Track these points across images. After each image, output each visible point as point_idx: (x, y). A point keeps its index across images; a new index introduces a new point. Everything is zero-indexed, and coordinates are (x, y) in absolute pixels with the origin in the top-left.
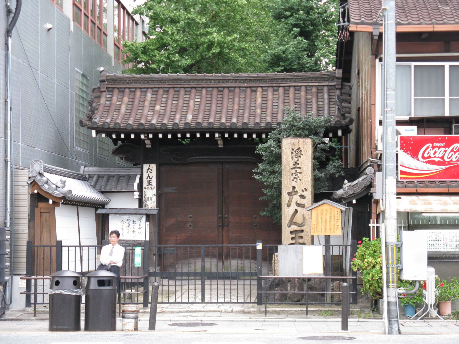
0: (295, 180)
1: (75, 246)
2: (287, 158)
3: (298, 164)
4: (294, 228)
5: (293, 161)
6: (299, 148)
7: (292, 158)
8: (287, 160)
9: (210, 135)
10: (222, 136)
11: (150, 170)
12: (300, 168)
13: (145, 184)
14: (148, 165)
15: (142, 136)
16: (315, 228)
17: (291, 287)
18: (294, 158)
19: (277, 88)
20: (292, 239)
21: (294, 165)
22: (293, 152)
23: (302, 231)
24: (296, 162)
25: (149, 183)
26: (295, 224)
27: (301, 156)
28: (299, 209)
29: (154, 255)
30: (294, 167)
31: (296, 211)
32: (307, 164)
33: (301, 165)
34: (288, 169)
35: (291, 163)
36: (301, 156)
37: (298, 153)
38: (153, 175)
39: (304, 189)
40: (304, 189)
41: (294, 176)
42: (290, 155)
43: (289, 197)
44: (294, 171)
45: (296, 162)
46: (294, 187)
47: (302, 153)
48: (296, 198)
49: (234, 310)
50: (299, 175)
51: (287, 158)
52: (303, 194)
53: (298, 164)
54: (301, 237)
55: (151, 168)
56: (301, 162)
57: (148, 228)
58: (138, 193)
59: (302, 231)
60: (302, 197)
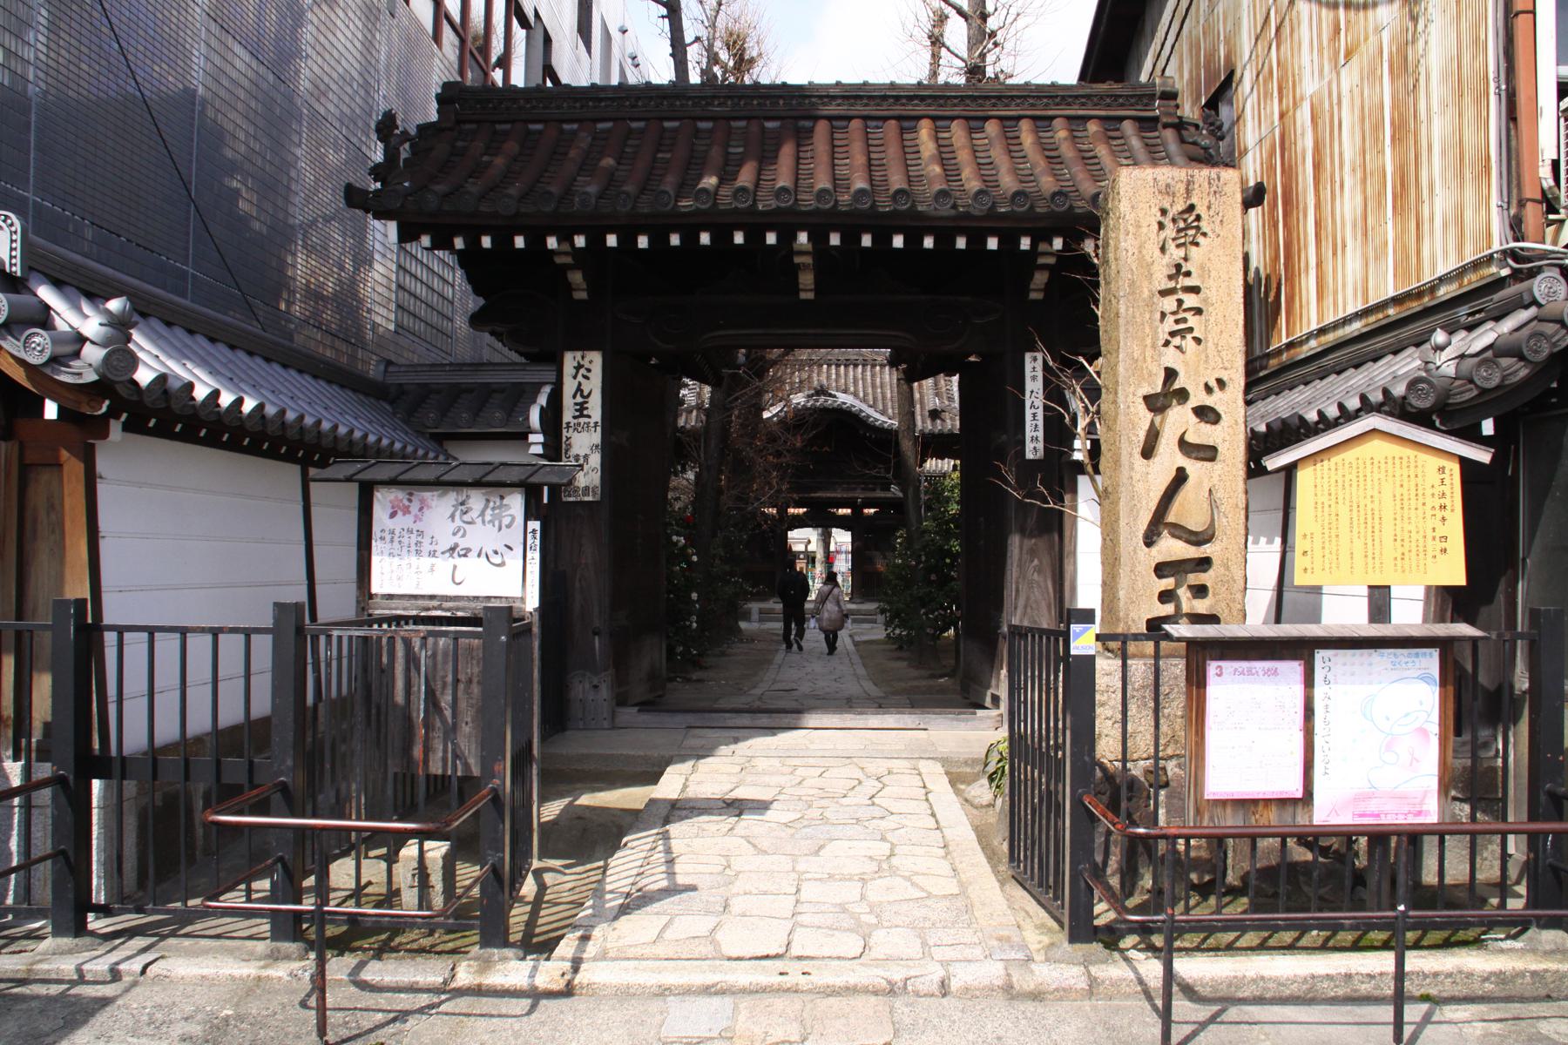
0: (1177, 341)
1: (248, 633)
2: (1141, 247)
3: (1188, 274)
4: (1171, 548)
5: (1166, 259)
6: (1191, 208)
7: (1163, 249)
8: (1141, 259)
9: (778, 239)
10: (819, 237)
11: (582, 371)
12: (1195, 290)
13: (568, 415)
14: (579, 354)
15: (552, 243)
16: (1318, 553)
17: (1168, 812)
18: (1171, 246)
19: (979, 124)
20: (1165, 597)
21: (1170, 277)
22: (1167, 221)
23: (1204, 563)
24: (1178, 267)
25: (581, 409)
26: (1179, 531)
27: (1200, 239)
28: (1193, 468)
29: (595, 634)
30: (1172, 284)
31: (1181, 477)
32: (1224, 276)
33: (1201, 276)
34: (1146, 294)
35: (1155, 267)
36: (1200, 239)
37: (1188, 228)
38: (594, 385)
39: (1213, 384)
40: (1213, 384)
41: (1169, 324)
42: (1153, 236)
43: (1149, 415)
44: (1169, 304)
45: (1178, 267)
46: (1171, 374)
47: (1204, 225)
48: (1179, 419)
49: (955, 985)
50: (1192, 320)
51: (1141, 247)
52: (1209, 401)
53: (1188, 274)
54: (1200, 591)
55: (587, 365)
56: (1202, 267)
57: (535, 542)
58: (540, 438)
59: (1204, 563)
60: (1206, 414)
